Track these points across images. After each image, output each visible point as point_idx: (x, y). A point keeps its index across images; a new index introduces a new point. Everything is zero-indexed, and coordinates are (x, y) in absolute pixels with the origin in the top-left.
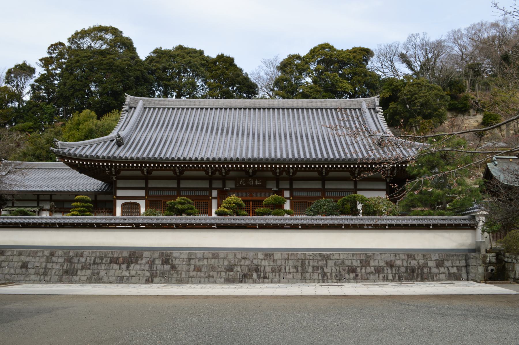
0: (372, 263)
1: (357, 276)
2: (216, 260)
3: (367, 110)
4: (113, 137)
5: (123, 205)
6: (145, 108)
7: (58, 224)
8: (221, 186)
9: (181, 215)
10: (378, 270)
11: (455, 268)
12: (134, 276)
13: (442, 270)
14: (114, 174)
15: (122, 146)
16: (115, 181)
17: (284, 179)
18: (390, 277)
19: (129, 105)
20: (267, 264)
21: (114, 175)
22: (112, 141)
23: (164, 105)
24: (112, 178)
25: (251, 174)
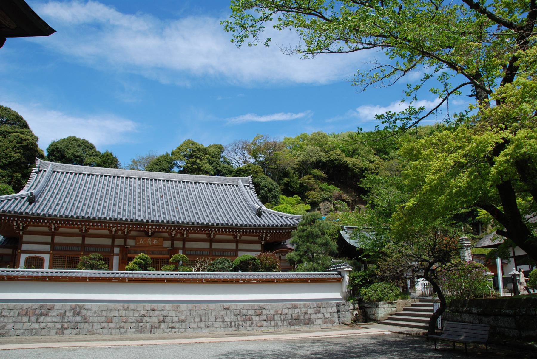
0: (265, 312)
1: (252, 323)
2: (127, 312)
3: (244, 188)
4: (24, 195)
5: (27, 259)
6: (54, 172)
7: (49, 277)
8: (122, 244)
9: (238, 272)
10: (270, 319)
11: (329, 314)
12: (44, 329)
13: (320, 315)
14: (21, 229)
15: (33, 204)
16: (22, 236)
17: (178, 240)
18: (280, 324)
19: (39, 167)
20: (174, 315)
21: (21, 230)
22: (24, 198)
23: (72, 170)
24: (19, 233)
25: (150, 234)
